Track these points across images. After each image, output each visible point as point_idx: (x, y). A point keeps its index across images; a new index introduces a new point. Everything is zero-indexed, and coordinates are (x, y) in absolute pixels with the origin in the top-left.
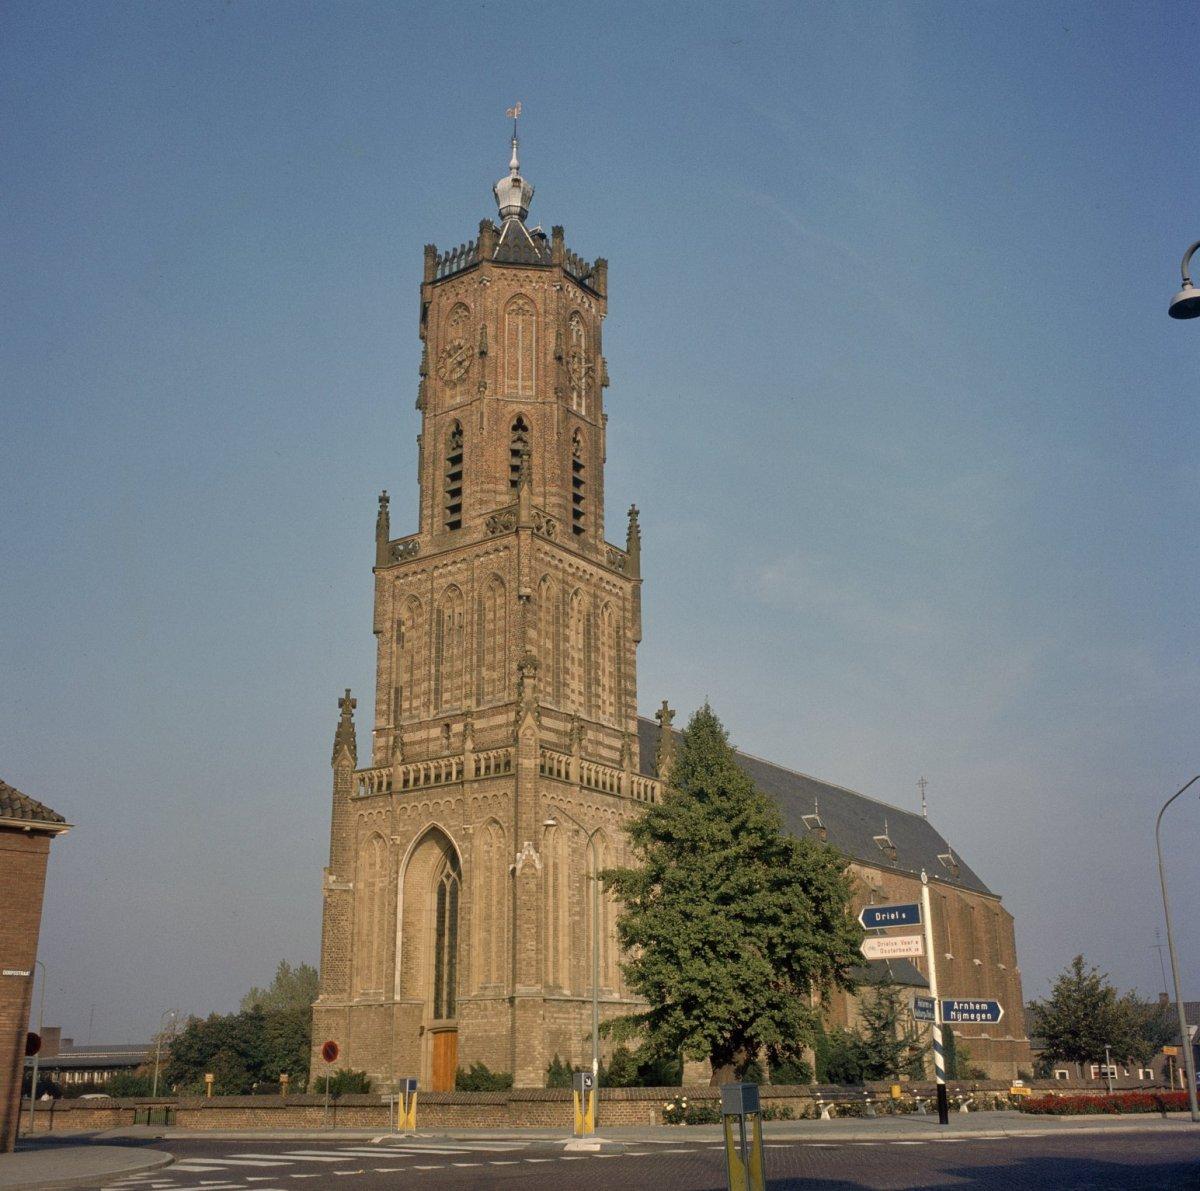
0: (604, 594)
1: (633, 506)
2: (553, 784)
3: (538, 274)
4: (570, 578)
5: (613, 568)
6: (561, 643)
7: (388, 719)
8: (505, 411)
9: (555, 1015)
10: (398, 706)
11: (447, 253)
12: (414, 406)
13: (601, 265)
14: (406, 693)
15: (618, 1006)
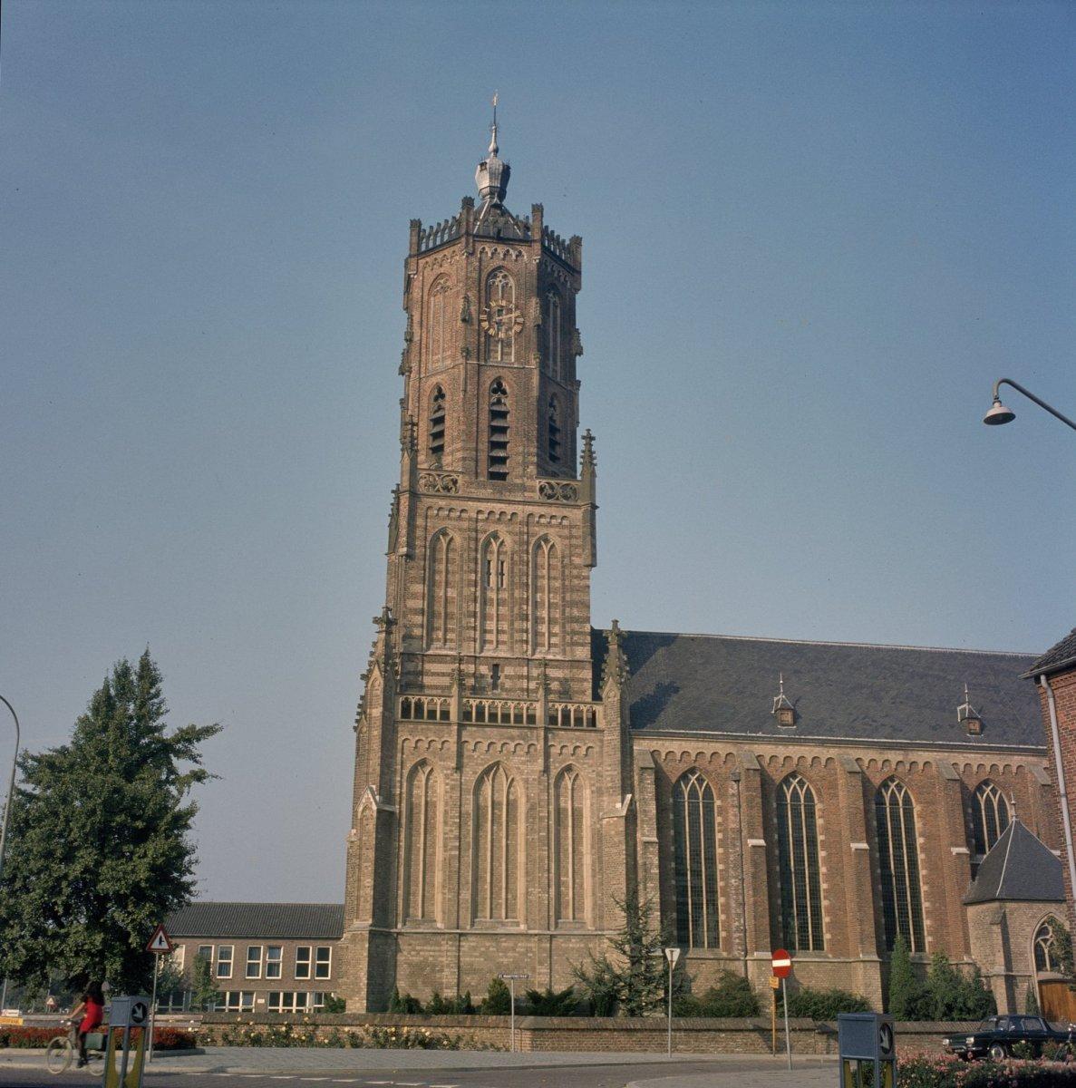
2: (420, 727)
9: (418, 948)
11: (431, 227)
15: (522, 938)
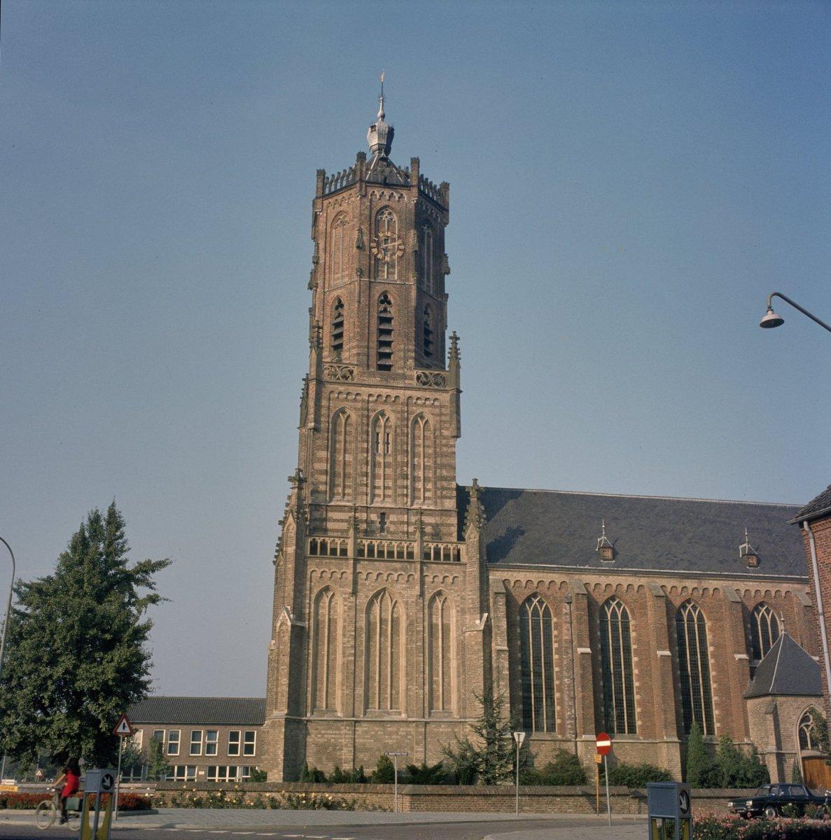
1: (455, 332)
2: (324, 561)
3: (349, 192)
9: (323, 732)
11: (333, 176)
15: (403, 724)
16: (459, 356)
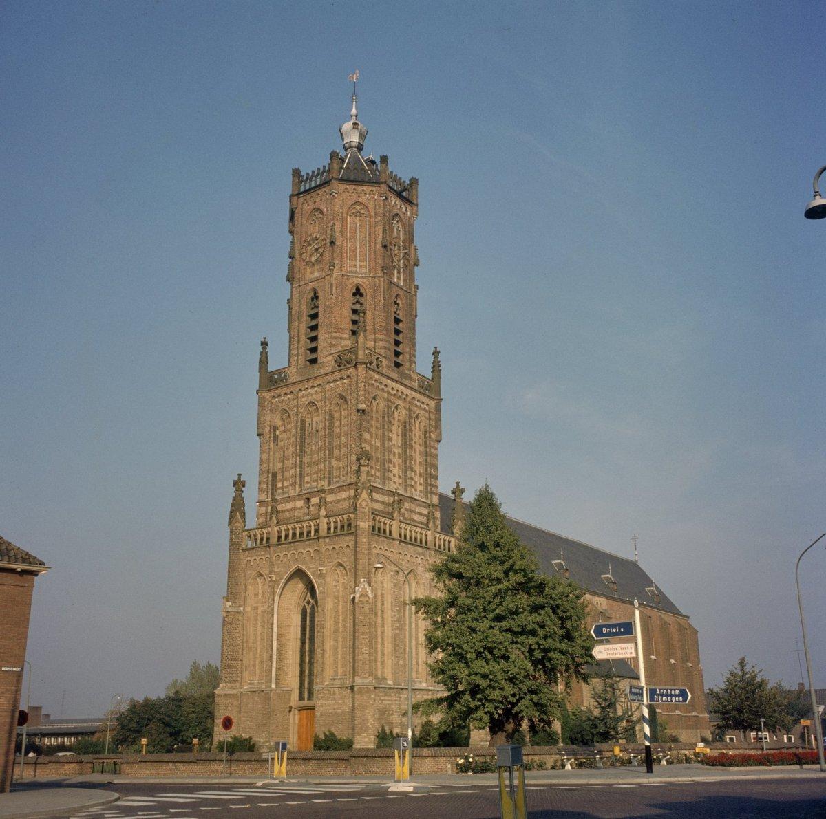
0: (416, 409)
1: (436, 348)
2: (380, 539)
4: (392, 397)
5: (422, 391)
6: (386, 442)
7: (267, 495)
8: (348, 283)
10: (274, 485)
11: (308, 174)
12: (285, 279)
13: (414, 182)
14: (279, 477)
15: (425, 692)
16: (440, 368)
